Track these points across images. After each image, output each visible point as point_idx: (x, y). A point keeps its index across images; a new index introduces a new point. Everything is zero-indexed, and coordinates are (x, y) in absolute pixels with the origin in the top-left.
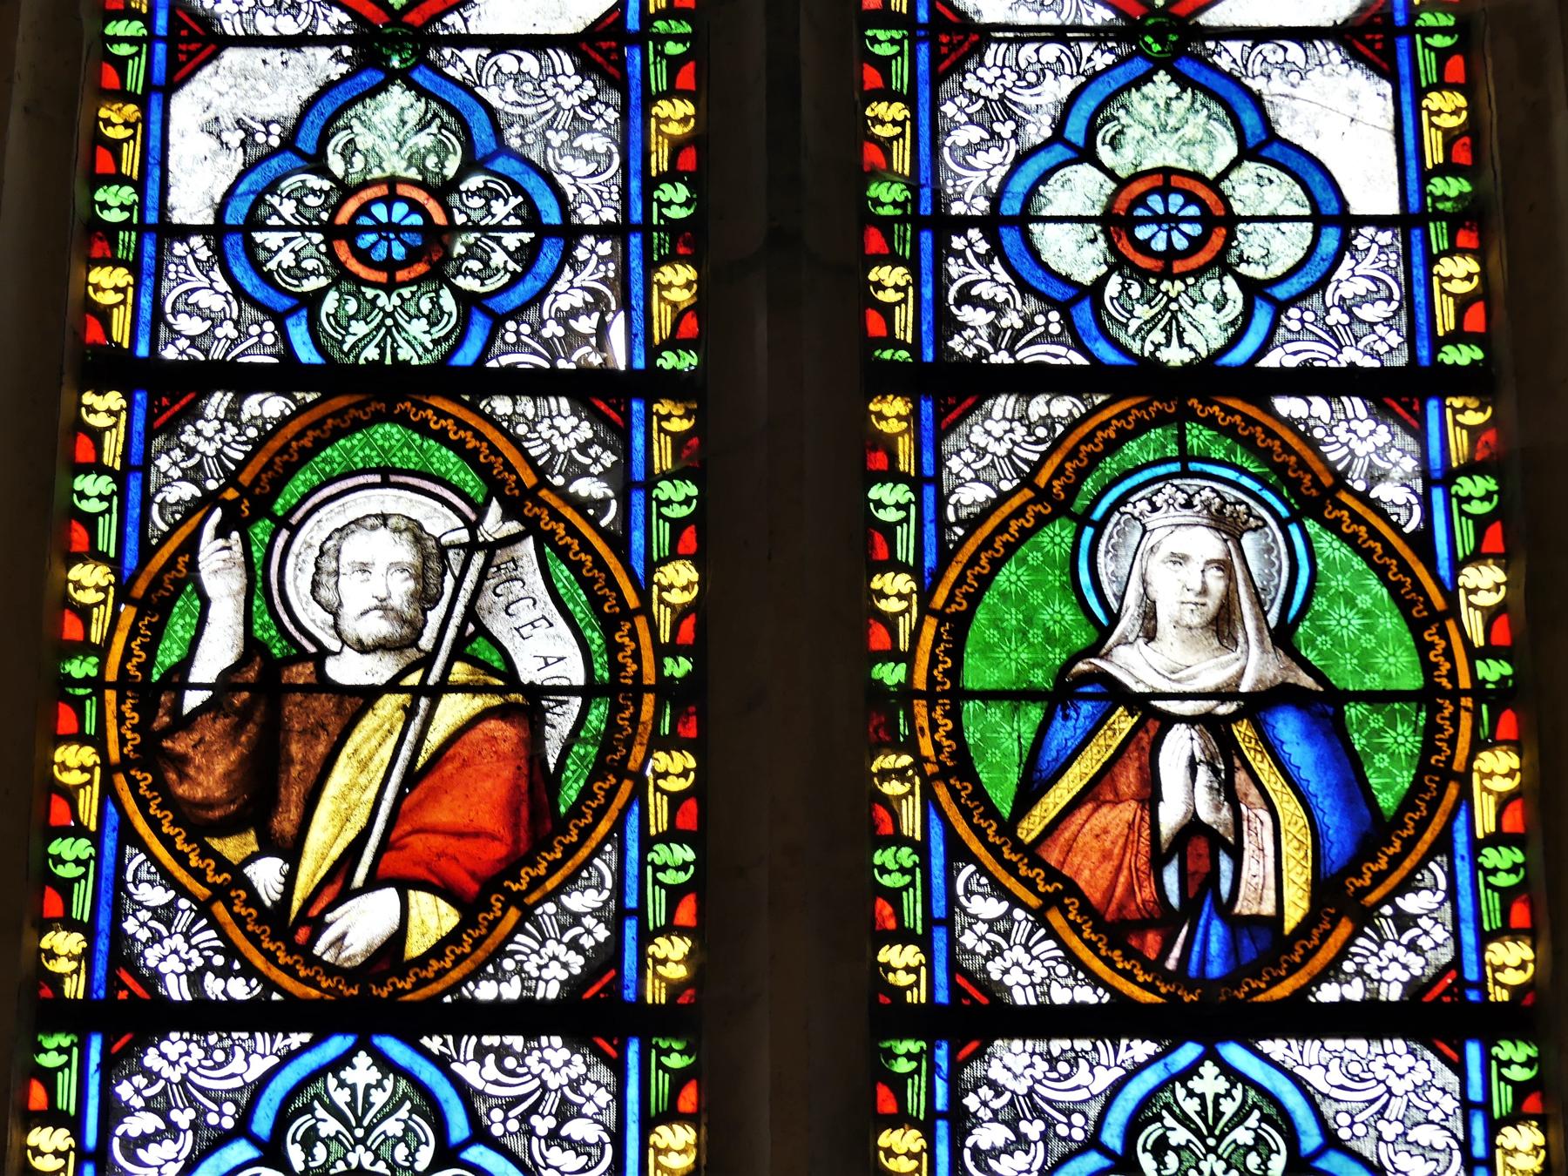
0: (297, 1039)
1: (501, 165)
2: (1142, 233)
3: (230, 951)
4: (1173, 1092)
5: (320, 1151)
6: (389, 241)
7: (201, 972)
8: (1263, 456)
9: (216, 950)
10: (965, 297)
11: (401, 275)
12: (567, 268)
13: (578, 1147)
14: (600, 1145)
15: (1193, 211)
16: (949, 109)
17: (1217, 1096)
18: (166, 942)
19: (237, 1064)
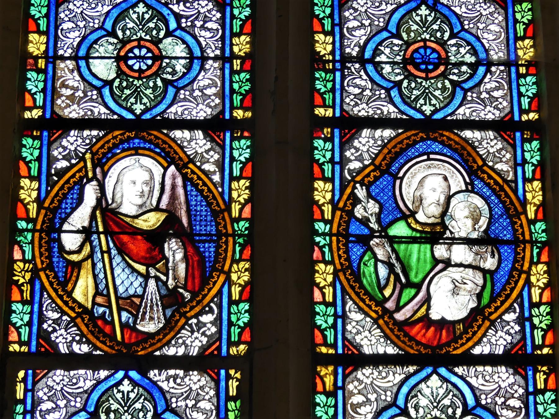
0: (412, 369)
1: (178, 33)
2: (130, 62)
3: (82, 335)
4: (113, 391)
5: (421, 411)
6: (140, 62)
7: (71, 342)
8: (449, 147)
9: (77, 335)
10: (64, 85)
11: (431, 75)
12: (489, 74)
13: (513, 409)
14: (520, 408)
15: (150, 55)
16: (62, 15)
17: (128, 392)
18: (58, 332)
19: (391, 377)
